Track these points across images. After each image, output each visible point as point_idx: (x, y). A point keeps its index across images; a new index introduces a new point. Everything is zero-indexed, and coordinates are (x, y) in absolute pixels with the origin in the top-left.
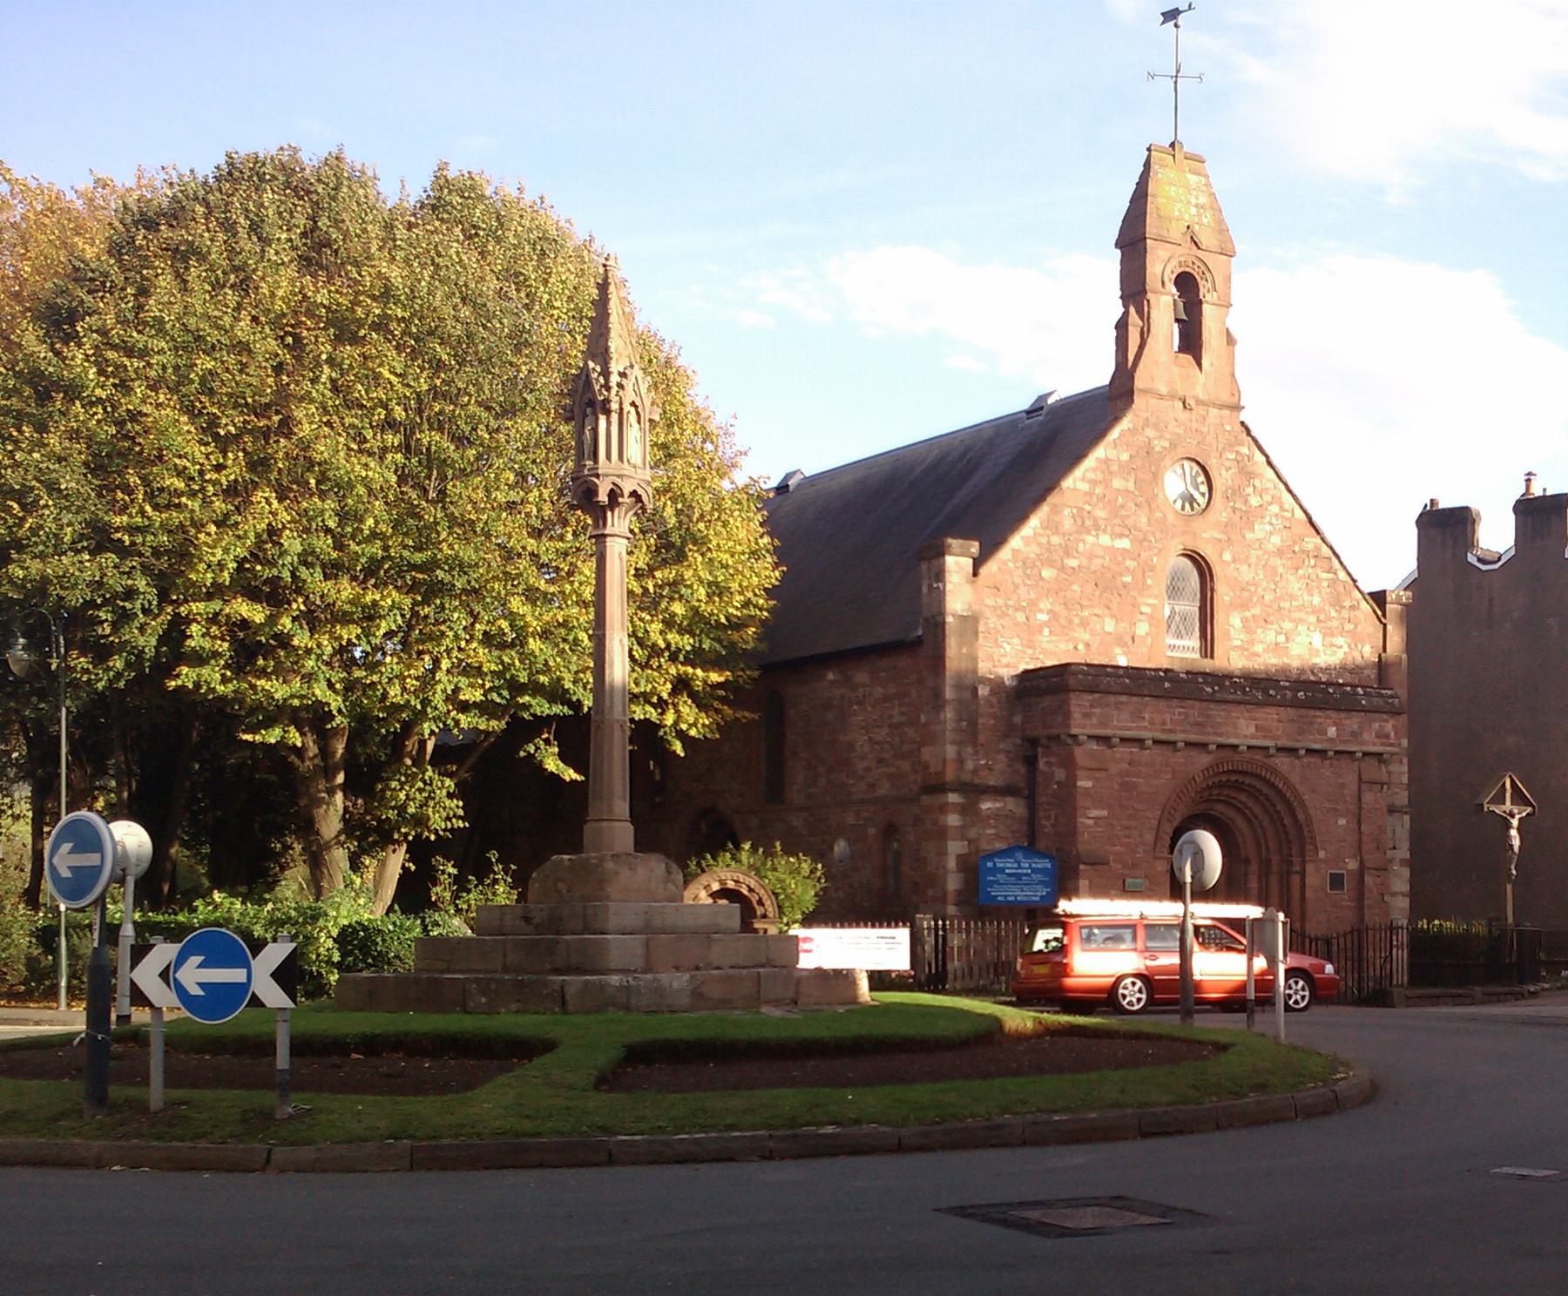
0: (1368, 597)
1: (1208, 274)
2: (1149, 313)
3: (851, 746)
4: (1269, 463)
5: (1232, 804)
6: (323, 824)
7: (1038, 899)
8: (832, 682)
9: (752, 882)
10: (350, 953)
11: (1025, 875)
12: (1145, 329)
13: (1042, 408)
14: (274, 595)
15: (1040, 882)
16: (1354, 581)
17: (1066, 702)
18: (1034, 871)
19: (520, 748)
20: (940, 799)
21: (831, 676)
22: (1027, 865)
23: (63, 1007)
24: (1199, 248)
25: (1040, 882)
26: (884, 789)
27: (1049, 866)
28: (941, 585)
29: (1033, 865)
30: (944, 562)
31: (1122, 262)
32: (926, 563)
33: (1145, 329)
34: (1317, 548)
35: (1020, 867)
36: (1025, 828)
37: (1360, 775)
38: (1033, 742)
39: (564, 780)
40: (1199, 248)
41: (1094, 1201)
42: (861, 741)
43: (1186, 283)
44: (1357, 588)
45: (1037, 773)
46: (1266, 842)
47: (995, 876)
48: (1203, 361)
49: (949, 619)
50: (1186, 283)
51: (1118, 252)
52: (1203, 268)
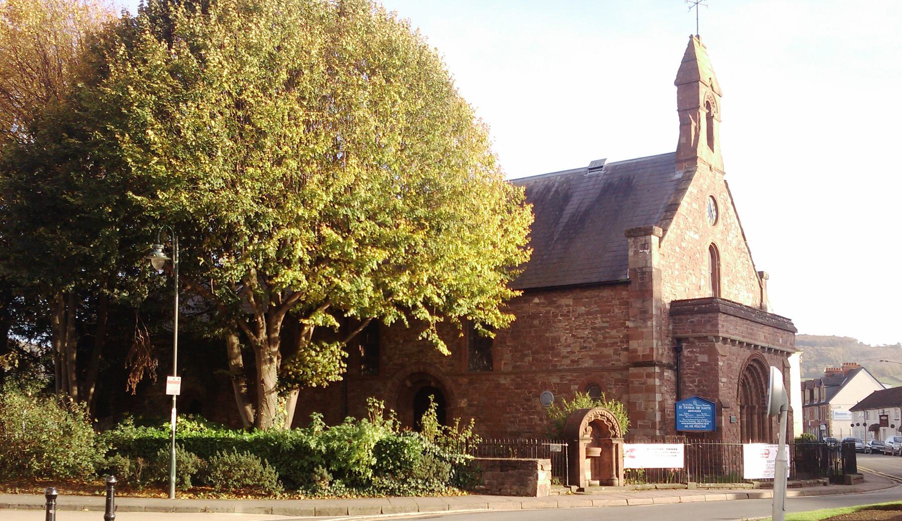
0: (758, 274)
1: (715, 104)
2: (699, 119)
3: (557, 340)
4: (733, 203)
5: (896, 378)
6: (267, 376)
7: (705, 427)
8: (537, 304)
9: (611, 416)
10: (385, 459)
11: (699, 413)
12: (698, 127)
13: (602, 167)
14: (342, 226)
15: (706, 417)
16: (754, 266)
17: (716, 318)
18: (703, 411)
19: (418, 333)
20: (650, 370)
21: (536, 300)
22: (699, 408)
23: (173, 497)
24: (713, 90)
25: (706, 417)
26: (588, 363)
27: (710, 408)
28: (647, 251)
29: (702, 408)
30: (651, 238)
31: (678, 92)
32: (633, 239)
33: (698, 127)
34: (744, 248)
35: (695, 409)
36: (674, 387)
37: (783, 363)
38: (679, 340)
39: (444, 355)
40: (713, 90)
41: (94, 508)
42: (565, 337)
43: (708, 105)
44: (754, 269)
45: (681, 357)
46: (751, 395)
47: (683, 414)
48: (714, 147)
49: (653, 270)
50: (708, 105)
51: (676, 88)
52: (714, 101)
